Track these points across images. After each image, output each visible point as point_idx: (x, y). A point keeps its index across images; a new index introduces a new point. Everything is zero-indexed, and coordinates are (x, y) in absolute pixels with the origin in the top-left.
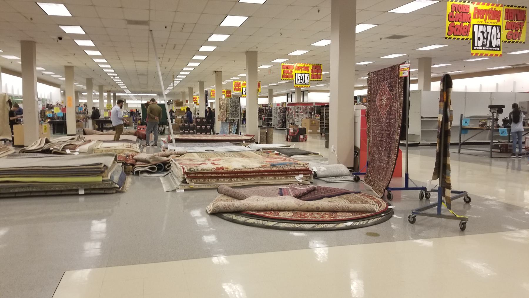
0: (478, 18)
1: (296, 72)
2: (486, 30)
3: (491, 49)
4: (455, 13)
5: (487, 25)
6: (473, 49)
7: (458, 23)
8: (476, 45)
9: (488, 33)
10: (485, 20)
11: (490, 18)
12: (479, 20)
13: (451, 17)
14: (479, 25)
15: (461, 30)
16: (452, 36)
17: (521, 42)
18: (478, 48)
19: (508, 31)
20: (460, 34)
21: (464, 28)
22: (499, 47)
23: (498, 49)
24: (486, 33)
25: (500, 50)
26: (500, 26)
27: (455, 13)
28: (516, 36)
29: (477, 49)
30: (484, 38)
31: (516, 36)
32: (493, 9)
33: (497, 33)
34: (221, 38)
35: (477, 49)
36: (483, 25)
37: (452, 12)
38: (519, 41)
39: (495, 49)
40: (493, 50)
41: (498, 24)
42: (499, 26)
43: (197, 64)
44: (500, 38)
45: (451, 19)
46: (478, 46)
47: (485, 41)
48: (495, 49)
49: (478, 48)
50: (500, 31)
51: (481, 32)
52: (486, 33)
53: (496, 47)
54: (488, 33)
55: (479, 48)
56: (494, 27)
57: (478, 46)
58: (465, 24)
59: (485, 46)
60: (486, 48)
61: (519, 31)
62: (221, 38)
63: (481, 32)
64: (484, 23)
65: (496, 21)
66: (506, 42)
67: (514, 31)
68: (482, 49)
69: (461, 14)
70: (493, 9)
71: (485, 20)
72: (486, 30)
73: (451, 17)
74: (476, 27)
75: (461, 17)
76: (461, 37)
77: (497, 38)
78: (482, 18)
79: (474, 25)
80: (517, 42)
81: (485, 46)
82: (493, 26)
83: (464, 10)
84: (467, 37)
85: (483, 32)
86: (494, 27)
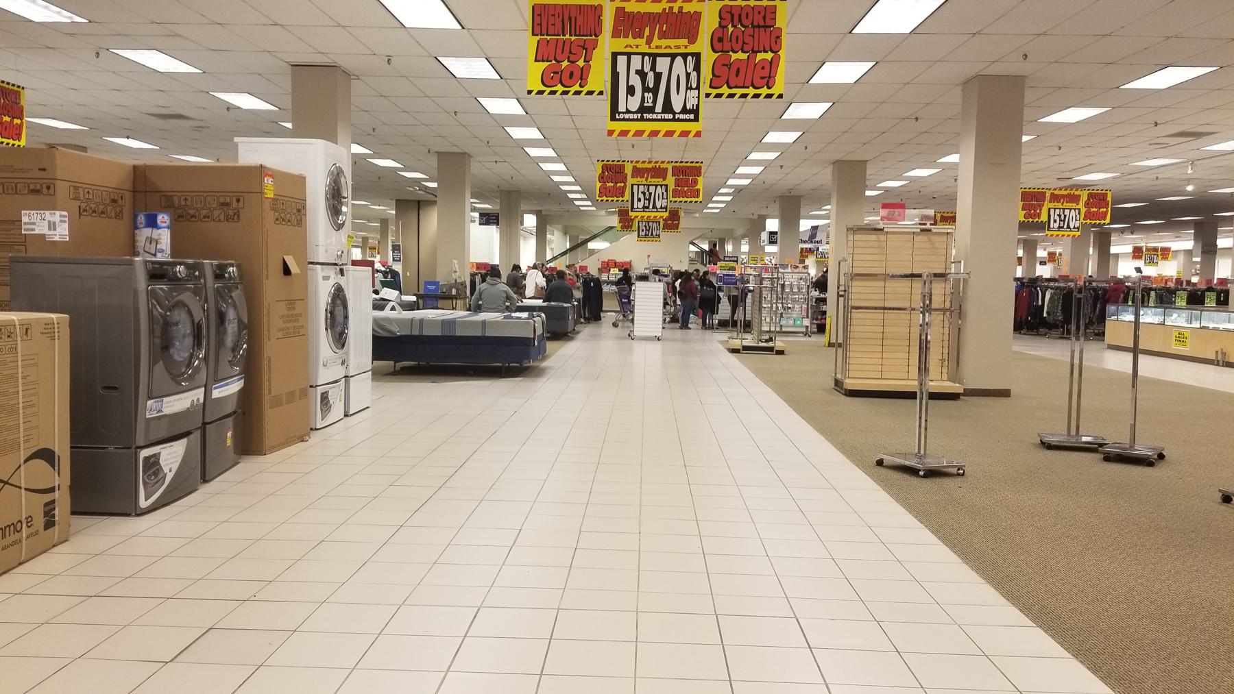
0: (626, 36)
1: (634, 181)
2: (653, 68)
3: (671, 116)
4: (731, 29)
5: (654, 57)
6: (613, 118)
7: (741, 56)
8: (622, 108)
9: (658, 76)
10: (649, 42)
11: (663, 35)
12: (630, 41)
13: (720, 40)
14: (629, 55)
15: (750, 72)
16: (725, 90)
17: (590, 93)
18: (627, 116)
19: (544, 65)
20: (748, 83)
21: (758, 68)
22: (696, 112)
23: (692, 117)
24: (651, 76)
25: (696, 119)
26: (697, 56)
27: (731, 29)
28: (571, 77)
29: (624, 120)
30: (645, 89)
31: (571, 77)
32: (676, 10)
33: (688, 75)
34: (811, 111)
35: (624, 120)
36: (643, 55)
37: (722, 26)
38: (585, 90)
39: (681, 116)
40: (674, 120)
41: (692, 49)
42: (692, 55)
43: (756, 170)
44: (698, 88)
45: (718, 46)
46: (628, 111)
47: (649, 96)
48: (681, 116)
49: (627, 116)
50: (697, 68)
51: (637, 72)
52: (651, 76)
53: (684, 110)
54: (658, 76)
55: (631, 116)
56: (679, 60)
57: (628, 111)
58: (760, 56)
59: (651, 110)
60: (655, 116)
61: (581, 63)
62: (811, 111)
63: (637, 72)
64: (644, 48)
65: (685, 42)
66: (541, 92)
67: (565, 64)
68: (642, 119)
69: (750, 31)
70: (676, 10)
71: (649, 42)
72: (653, 68)
73: (720, 40)
74: (635, 187)
75: (748, 40)
76: (751, 91)
77: (689, 88)
78: (640, 36)
79: (615, 56)
80: (577, 93)
81: (651, 110)
82: (673, 57)
83: (759, 20)
84: (770, 92)
85: (644, 193)
86: (679, 60)
